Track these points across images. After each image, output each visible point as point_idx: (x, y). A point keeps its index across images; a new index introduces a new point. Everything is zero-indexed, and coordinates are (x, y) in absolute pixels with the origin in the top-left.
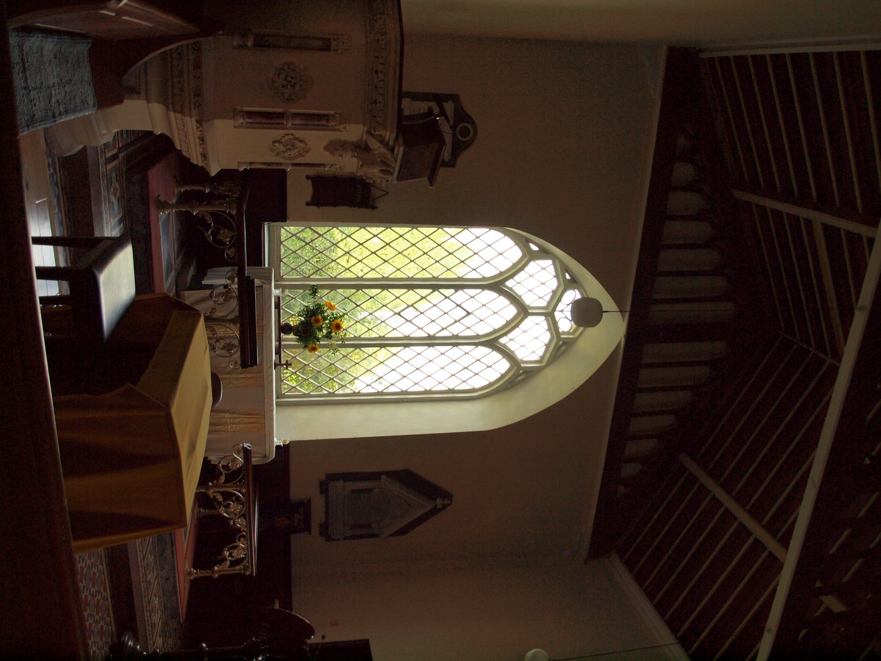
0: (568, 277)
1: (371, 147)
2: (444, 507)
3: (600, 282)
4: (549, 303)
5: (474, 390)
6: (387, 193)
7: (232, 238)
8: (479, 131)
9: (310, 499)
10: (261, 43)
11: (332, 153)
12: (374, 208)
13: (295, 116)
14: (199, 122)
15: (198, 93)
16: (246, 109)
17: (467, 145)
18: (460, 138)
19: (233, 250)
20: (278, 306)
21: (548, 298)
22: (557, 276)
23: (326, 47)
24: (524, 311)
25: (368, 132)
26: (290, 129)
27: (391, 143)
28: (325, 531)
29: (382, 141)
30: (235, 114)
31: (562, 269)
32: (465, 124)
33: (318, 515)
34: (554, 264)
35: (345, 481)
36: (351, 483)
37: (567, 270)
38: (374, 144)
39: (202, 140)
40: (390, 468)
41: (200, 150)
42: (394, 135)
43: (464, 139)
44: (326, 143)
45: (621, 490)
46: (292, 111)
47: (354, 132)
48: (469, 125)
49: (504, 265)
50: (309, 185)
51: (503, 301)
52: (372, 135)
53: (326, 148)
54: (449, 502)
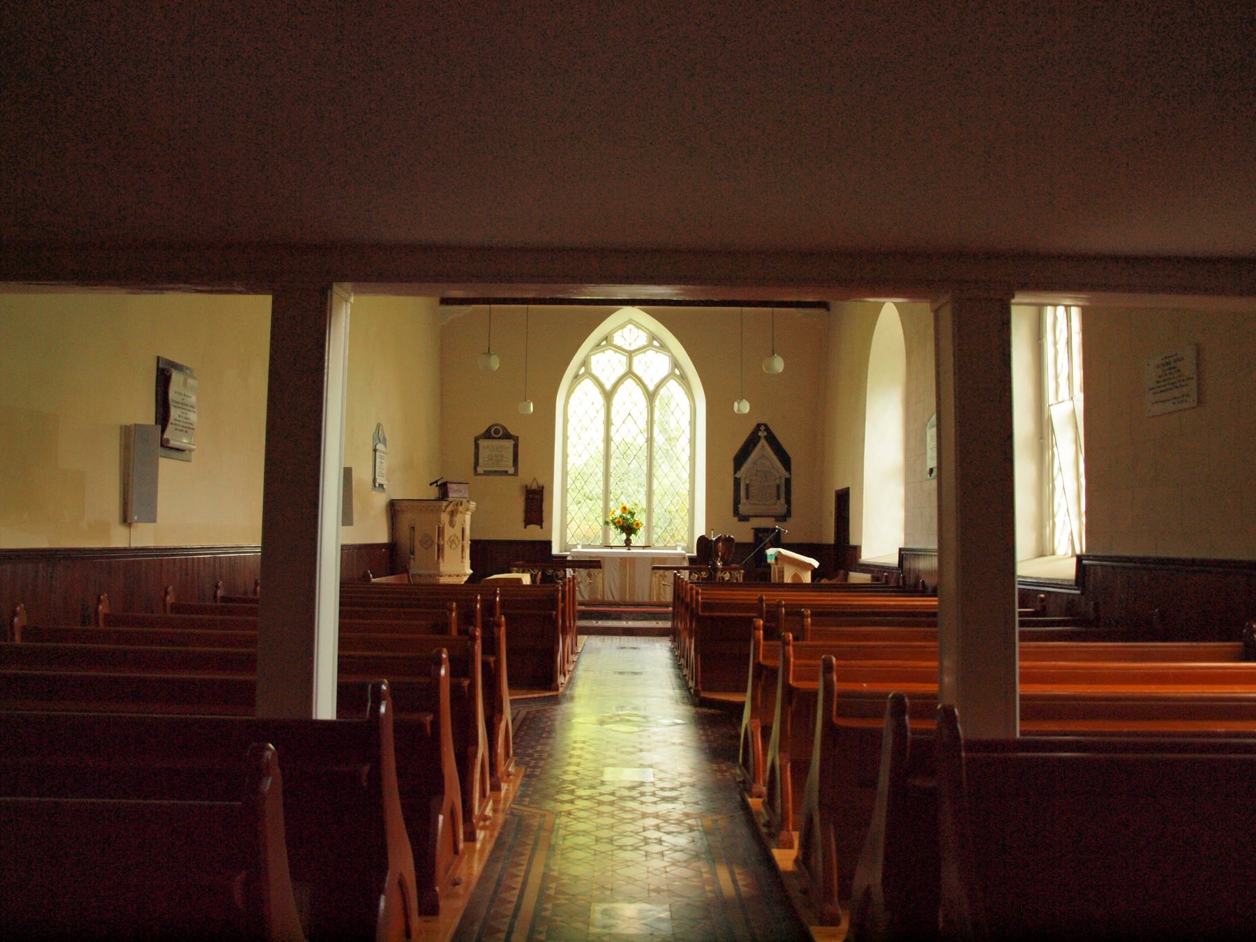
0: (604, 343)
2: (767, 429)
4: (624, 355)
6: (535, 479)
7: (695, 573)
8: (497, 422)
9: (753, 529)
10: (412, 553)
12: (543, 487)
13: (438, 540)
14: (441, 576)
16: (436, 558)
17: (504, 428)
20: (589, 546)
24: (630, 373)
25: (444, 511)
28: (783, 518)
29: (447, 507)
30: (438, 563)
32: (492, 432)
34: (594, 354)
35: (739, 503)
36: (741, 501)
37: (598, 345)
38: (449, 509)
39: (450, 576)
40: (732, 473)
41: (455, 577)
43: (501, 432)
44: (451, 528)
46: (436, 541)
47: (445, 517)
48: (493, 429)
49: (596, 391)
51: (621, 390)
53: (453, 527)
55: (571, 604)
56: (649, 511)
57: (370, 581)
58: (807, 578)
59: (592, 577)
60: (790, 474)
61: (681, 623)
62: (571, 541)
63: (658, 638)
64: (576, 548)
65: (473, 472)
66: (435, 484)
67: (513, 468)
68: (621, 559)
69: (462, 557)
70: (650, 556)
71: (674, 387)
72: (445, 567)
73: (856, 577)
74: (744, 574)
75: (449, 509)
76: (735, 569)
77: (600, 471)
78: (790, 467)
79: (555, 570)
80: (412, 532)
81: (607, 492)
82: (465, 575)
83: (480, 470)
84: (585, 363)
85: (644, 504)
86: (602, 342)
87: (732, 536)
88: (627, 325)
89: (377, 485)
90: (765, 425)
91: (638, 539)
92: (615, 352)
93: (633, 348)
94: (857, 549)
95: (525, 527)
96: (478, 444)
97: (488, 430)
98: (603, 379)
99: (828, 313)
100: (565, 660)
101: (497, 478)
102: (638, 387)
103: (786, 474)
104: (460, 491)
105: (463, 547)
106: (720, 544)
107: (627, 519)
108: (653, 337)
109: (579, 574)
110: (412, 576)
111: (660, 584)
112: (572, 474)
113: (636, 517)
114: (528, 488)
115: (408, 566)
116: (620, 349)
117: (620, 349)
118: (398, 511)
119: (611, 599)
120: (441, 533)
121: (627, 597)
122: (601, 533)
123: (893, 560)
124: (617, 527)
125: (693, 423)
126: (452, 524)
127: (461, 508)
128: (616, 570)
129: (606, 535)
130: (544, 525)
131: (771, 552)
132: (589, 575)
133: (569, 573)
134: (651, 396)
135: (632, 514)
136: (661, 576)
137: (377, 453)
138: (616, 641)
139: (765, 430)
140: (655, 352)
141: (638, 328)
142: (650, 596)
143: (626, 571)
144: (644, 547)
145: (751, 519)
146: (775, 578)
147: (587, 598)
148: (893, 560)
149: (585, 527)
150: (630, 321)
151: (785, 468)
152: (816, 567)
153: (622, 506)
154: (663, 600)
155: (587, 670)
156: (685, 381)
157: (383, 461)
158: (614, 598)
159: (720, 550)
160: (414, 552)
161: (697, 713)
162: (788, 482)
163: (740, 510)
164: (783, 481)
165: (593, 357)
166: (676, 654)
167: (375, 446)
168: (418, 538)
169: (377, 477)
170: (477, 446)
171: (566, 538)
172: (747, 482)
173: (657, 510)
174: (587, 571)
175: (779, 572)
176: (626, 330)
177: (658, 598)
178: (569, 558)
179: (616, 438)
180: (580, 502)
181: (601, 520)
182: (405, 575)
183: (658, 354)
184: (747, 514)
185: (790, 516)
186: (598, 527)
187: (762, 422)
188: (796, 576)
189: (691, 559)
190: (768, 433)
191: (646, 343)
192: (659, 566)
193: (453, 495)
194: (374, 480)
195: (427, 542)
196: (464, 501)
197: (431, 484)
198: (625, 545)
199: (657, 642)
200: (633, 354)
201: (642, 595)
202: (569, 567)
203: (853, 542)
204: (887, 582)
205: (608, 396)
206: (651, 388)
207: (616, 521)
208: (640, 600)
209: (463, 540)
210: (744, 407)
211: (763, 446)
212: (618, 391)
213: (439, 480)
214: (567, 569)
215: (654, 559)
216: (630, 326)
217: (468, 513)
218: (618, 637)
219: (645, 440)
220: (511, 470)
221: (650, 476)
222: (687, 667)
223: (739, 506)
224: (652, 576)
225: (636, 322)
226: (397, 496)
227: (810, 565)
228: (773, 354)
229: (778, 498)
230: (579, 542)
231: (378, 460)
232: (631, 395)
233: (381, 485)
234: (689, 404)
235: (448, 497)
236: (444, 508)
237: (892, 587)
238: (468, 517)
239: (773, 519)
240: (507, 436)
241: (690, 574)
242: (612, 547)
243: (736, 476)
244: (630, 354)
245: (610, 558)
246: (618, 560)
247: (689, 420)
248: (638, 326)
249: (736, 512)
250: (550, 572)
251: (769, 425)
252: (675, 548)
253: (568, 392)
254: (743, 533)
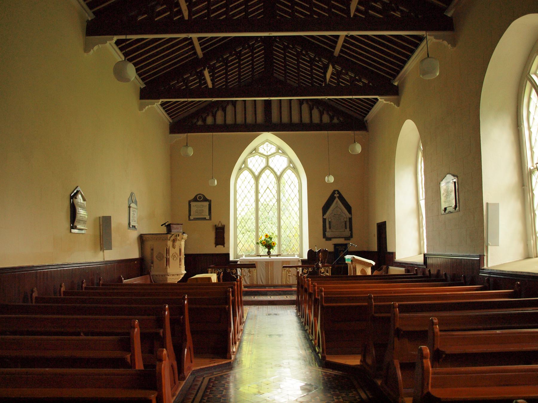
0: (254, 152)
1: (173, 239)
2: (339, 193)
4: (264, 158)
5: (299, 182)
6: (220, 222)
7: (306, 269)
10: (152, 263)
11: (175, 247)
12: (224, 226)
13: (166, 256)
14: (168, 275)
15: (162, 276)
18: (202, 199)
19: (309, 269)
20: (249, 256)
21: (262, 158)
22: (254, 156)
23: (152, 250)
24: (267, 167)
25: (169, 240)
26: (169, 256)
27: (171, 235)
28: (348, 238)
29: (171, 237)
30: (166, 268)
32: (198, 198)
33: (341, 241)
37: (251, 153)
38: (172, 238)
39: (173, 275)
40: (321, 214)
41: (176, 276)
42: (170, 235)
43: (202, 198)
45: (335, 121)
46: (165, 256)
47: (170, 243)
49: (250, 176)
51: (263, 175)
52: (170, 239)
53: (174, 249)
54: (336, 191)
55: (239, 292)
58: (369, 272)
59: (251, 273)
60: (351, 215)
62: (240, 253)
64: (242, 257)
66: (164, 225)
68: (266, 262)
69: (180, 265)
70: (281, 260)
72: (170, 270)
73: (394, 270)
74: (331, 269)
75: (172, 238)
76: (327, 266)
77: (253, 217)
79: (231, 269)
80: (152, 252)
81: (257, 227)
82: (182, 274)
83: (192, 218)
84: (244, 162)
85: (276, 233)
86: (253, 151)
87: (327, 249)
89: (131, 226)
90: (338, 191)
91: (274, 252)
93: (269, 154)
94: (393, 254)
95: (216, 247)
96: (191, 204)
98: (254, 170)
99: (368, 133)
100: (236, 332)
103: (349, 216)
104: (178, 229)
107: (269, 241)
108: (279, 148)
109: (244, 271)
110: (152, 276)
111: (286, 274)
112: (239, 218)
113: (273, 240)
114: (217, 227)
118: (145, 240)
119: (261, 283)
120: (168, 251)
122: (255, 248)
123: (420, 260)
124: (263, 245)
125: (300, 191)
126: (174, 247)
127: (178, 238)
129: (257, 249)
130: (225, 245)
131: (348, 257)
132: (249, 272)
133: (239, 270)
134: (279, 178)
135: (271, 238)
136: (288, 271)
137: (131, 209)
138: (265, 309)
139: (338, 193)
140: (280, 156)
141: (271, 144)
143: (269, 268)
144: (277, 255)
146: (351, 273)
147: (248, 283)
148: (420, 260)
149: (246, 246)
150: (267, 141)
151: (349, 213)
152: (374, 265)
153: (265, 234)
154: (288, 283)
155: (250, 334)
156: (296, 170)
164: (348, 220)
165: (248, 159)
166: (302, 321)
167: (130, 205)
169: (131, 222)
171: (237, 252)
173: (283, 236)
175: (354, 268)
176: (265, 145)
177: (286, 282)
178: (239, 263)
180: (244, 233)
181: (255, 242)
182: (148, 276)
184: (330, 237)
186: (253, 245)
188: (363, 271)
189: (303, 261)
191: (275, 152)
192: (287, 266)
193: (174, 231)
194: (129, 224)
195: (160, 257)
196: (180, 234)
198: (267, 254)
199: (288, 309)
203: (389, 250)
205: (257, 178)
207: (263, 242)
208: (277, 283)
209: (180, 255)
210: (331, 179)
211: (337, 201)
212: (260, 182)
213: (166, 223)
214: (238, 269)
215: (283, 262)
216: (267, 143)
218: (266, 306)
219: (276, 200)
220: (208, 217)
221: (279, 218)
222: (308, 325)
224: (282, 271)
225: (270, 141)
226: (145, 231)
227: (371, 264)
228: (355, 142)
229: (346, 228)
231: (131, 213)
232: (267, 179)
233: (134, 227)
235: (171, 232)
236: (169, 238)
237: (420, 277)
238: (183, 243)
239: (344, 239)
240: (205, 200)
241: (303, 270)
242: (261, 256)
243: (324, 217)
244: (267, 157)
246: (265, 263)
247: (298, 189)
248: (271, 143)
249: (324, 236)
250: (229, 270)
251: (340, 191)
252: (294, 255)
254: (329, 247)
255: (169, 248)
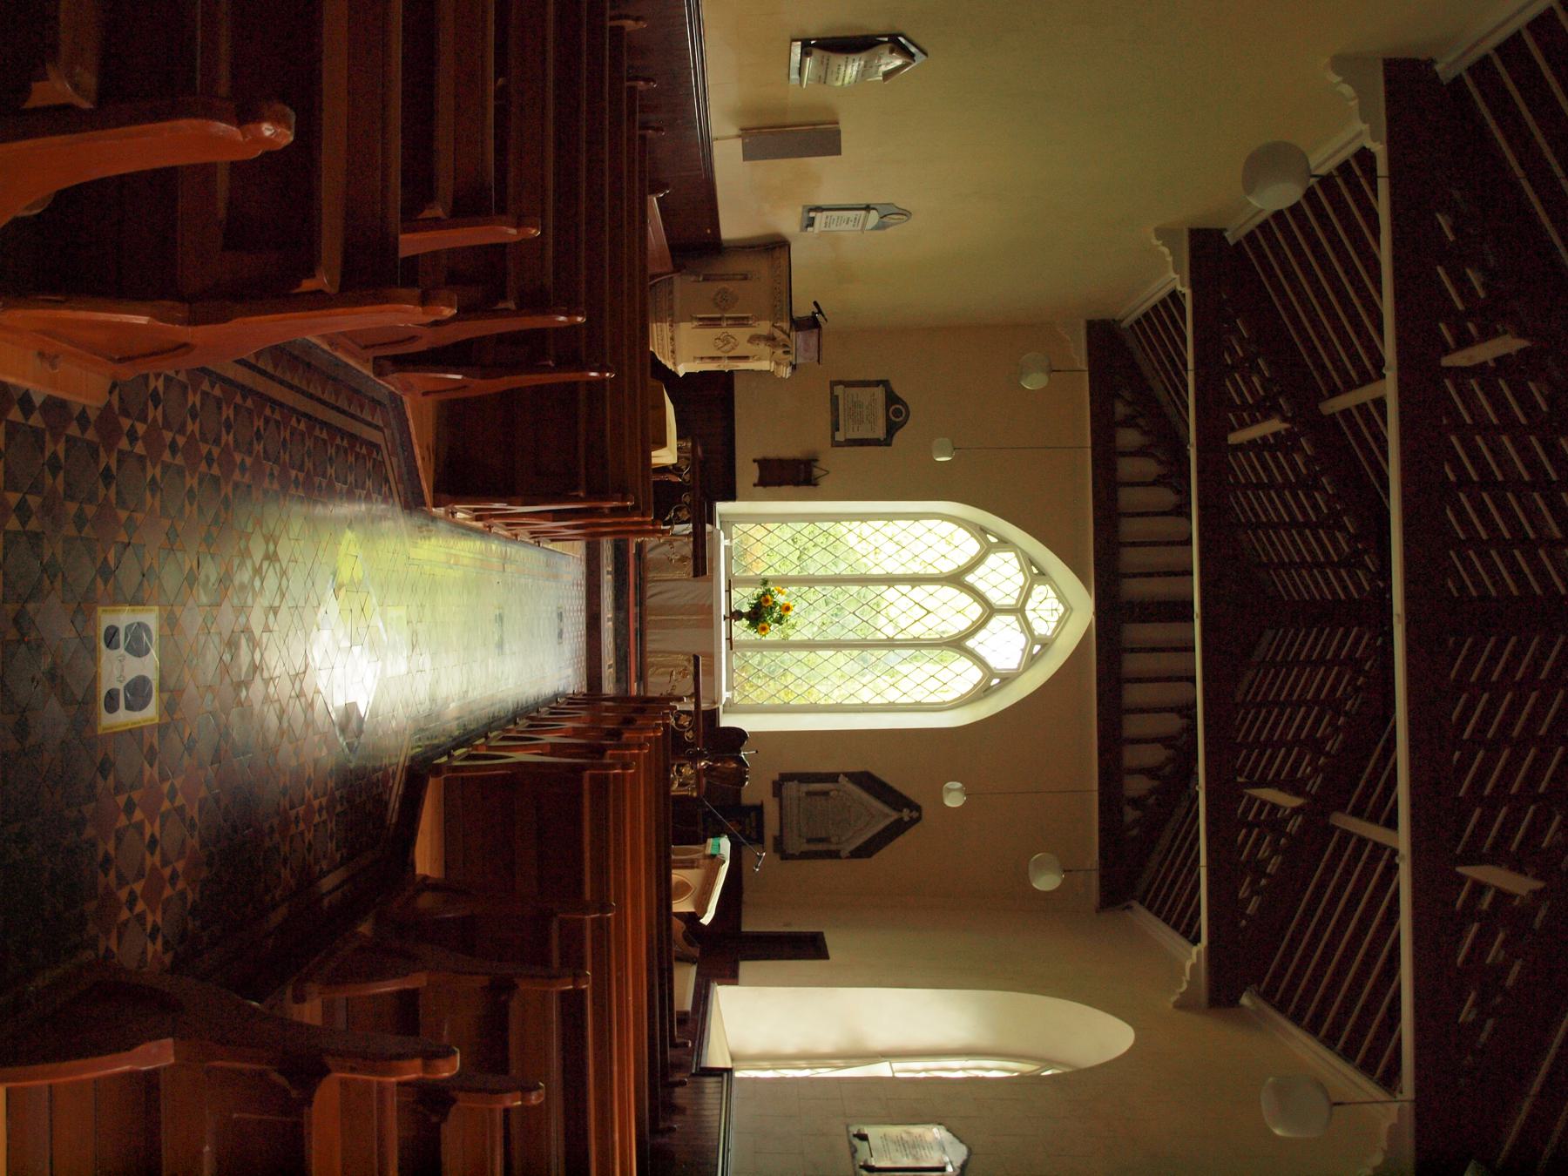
0: (1035, 571)
3: (1035, 536)
4: (1018, 600)
5: (944, 703)
6: (828, 472)
7: (690, 722)
10: (706, 279)
12: (815, 485)
13: (728, 319)
14: (671, 326)
15: (671, 307)
18: (893, 418)
19: (691, 732)
21: (1016, 595)
23: (745, 278)
24: (990, 611)
25: (773, 325)
28: (779, 846)
30: (692, 319)
31: (1029, 561)
33: (771, 827)
34: (1017, 556)
35: (800, 781)
36: (805, 785)
37: (1032, 562)
38: (777, 333)
39: (672, 339)
43: (897, 420)
44: (748, 337)
45: (1130, 814)
47: (764, 327)
49: (962, 559)
50: (755, 467)
51: (965, 599)
53: (749, 341)
56: (786, 645)
57: (654, 192)
58: (682, 906)
60: (847, 858)
61: (576, 732)
62: (736, 530)
63: (583, 670)
64: (725, 538)
65: (834, 378)
66: (816, 310)
67: (843, 439)
68: (711, 606)
69: (702, 358)
70: (716, 650)
71: (972, 676)
73: (685, 980)
74: (692, 796)
77: (842, 569)
78: (860, 857)
79: (689, 506)
81: (811, 581)
82: (675, 364)
83: (839, 390)
84: (1004, 543)
85: (795, 637)
88: (1063, 604)
89: (812, 214)
90: (919, 819)
91: (741, 629)
92: (1022, 588)
93: (1030, 615)
94: (732, 978)
95: (755, 461)
96: (878, 386)
97: (897, 400)
98: (981, 570)
100: (511, 521)
101: (827, 417)
102: (970, 623)
103: (846, 851)
104: (806, 350)
105: (719, 358)
106: (734, 765)
108: (1046, 644)
112: (841, 528)
115: (684, 271)
116: (1026, 594)
117: (1026, 594)
120: (740, 322)
121: (653, 618)
124: (759, 597)
126: (754, 339)
127: (779, 352)
128: (693, 599)
129: (747, 582)
131: (725, 845)
132: (683, 559)
133: (687, 528)
134: (957, 643)
135: (779, 621)
139: (911, 818)
141: (1059, 622)
142: (655, 652)
144: (730, 639)
145: (777, 799)
146: (679, 852)
147: (650, 556)
148: (716, 1056)
149: (759, 550)
150: (1069, 609)
153: (791, 604)
154: (650, 672)
155: (505, 559)
157: (851, 224)
158: (652, 596)
159: (726, 765)
160: (708, 280)
161: (386, 777)
162: (834, 855)
163: (790, 783)
164: (833, 847)
167: (874, 209)
168: (730, 286)
169: (825, 213)
170: (878, 383)
171: (740, 523)
172: (832, 793)
173: (787, 657)
174: (690, 556)
175: (692, 861)
178: (708, 527)
179: (891, 593)
180: (795, 543)
181: (770, 573)
182: (672, 268)
183: (1021, 653)
185: (782, 859)
186: (759, 570)
187: (924, 814)
188: (684, 888)
189: (713, 715)
190: (906, 823)
191: (1036, 633)
192: (700, 666)
193: (798, 338)
194: (819, 209)
195: (723, 301)
196: (791, 358)
197: (815, 303)
198: (733, 610)
199: (575, 671)
200: (1019, 615)
201: (656, 640)
202: (694, 527)
203: (745, 968)
204: (674, 1045)
205: (956, 579)
206: (970, 643)
207: (769, 597)
209: (730, 358)
210: (954, 798)
211: (887, 816)
215: (712, 657)
216: (1061, 609)
217: (773, 364)
218: (584, 607)
219: (891, 636)
220: (840, 437)
221: (838, 645)
223: (796, 782)
227: (704, 912)
230: (734, 541)
232: (954, 612)
233: (811, 222)
234: (947, 700)
238: (765, 365)
240: (892, 429)
241: (688, 713)
244: (1019, 610)
245: (711, 591)
246: (708, 603)
248: (1062, 622)
249: (786, 778)
251: (919, 824)
253: (955, 517)
254: (755, 790)
255: (751, 326)
